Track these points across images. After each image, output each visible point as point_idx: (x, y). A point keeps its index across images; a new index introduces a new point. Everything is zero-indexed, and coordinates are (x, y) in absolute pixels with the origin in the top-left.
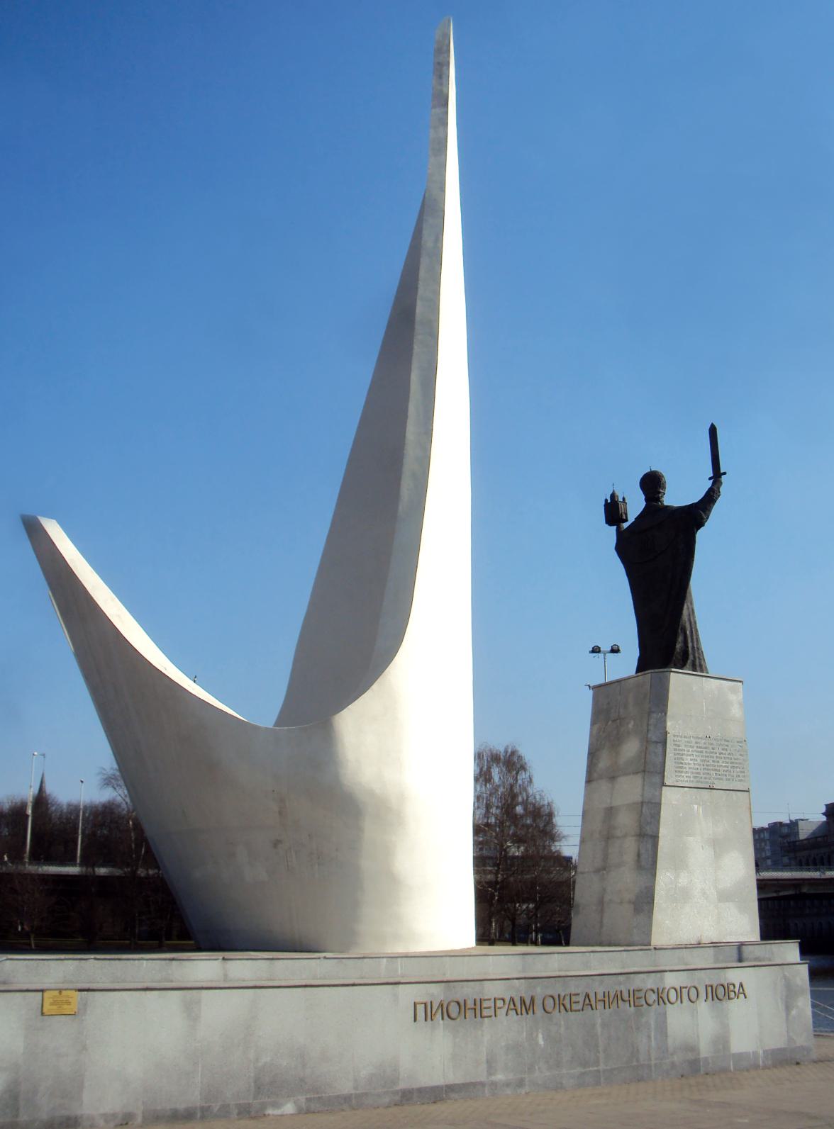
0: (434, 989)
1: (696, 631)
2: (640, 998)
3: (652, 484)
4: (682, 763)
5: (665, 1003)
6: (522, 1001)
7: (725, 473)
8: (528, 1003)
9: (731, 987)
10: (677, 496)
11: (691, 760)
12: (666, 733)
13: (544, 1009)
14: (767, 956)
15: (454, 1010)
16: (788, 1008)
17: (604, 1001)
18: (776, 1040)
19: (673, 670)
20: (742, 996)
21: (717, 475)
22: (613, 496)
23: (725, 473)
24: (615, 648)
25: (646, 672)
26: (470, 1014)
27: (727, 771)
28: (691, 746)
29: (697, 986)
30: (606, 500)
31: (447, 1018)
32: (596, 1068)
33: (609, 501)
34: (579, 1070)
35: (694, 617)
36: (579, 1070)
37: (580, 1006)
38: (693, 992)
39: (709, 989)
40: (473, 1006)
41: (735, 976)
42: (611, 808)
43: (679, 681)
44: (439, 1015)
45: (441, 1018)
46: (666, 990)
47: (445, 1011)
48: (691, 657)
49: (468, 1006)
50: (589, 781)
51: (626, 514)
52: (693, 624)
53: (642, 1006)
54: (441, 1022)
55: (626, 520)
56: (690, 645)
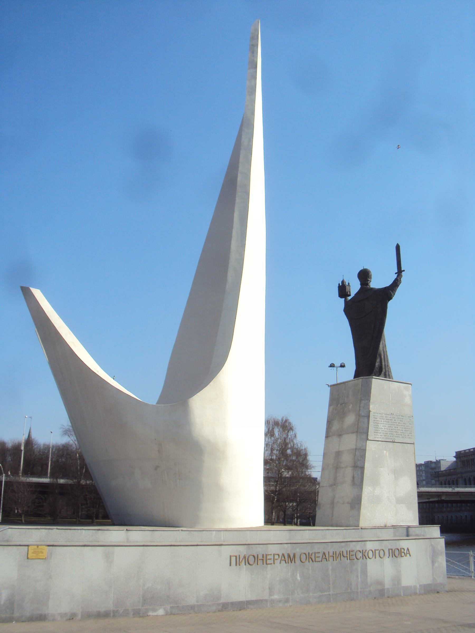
0: (241, 548)
4: (378, 428)
5: (366, 558)
7: (404, 271)
9: (403, 550)
12: (369, 411)
15: (251, 560)
17: (333, 557)
19: (374, 377)
21: (400, 271)
22: (343, 282)
23: (404, 271)
25: (359, 378)
27: (402, 432)
29: (384, 549)
30: (339, 284)
33: (341, 285)
34: (319, 594)
35: (386, 348)
36: (319, 594)
37: (320, 559)
38: (382, 553)
39: (391, 551)
48: (384, 370)
50: (327, 437)
51: (350, 292)
52: (385, 352)
53: (354, 559)
55: (350, 295)
56: (383, 364)
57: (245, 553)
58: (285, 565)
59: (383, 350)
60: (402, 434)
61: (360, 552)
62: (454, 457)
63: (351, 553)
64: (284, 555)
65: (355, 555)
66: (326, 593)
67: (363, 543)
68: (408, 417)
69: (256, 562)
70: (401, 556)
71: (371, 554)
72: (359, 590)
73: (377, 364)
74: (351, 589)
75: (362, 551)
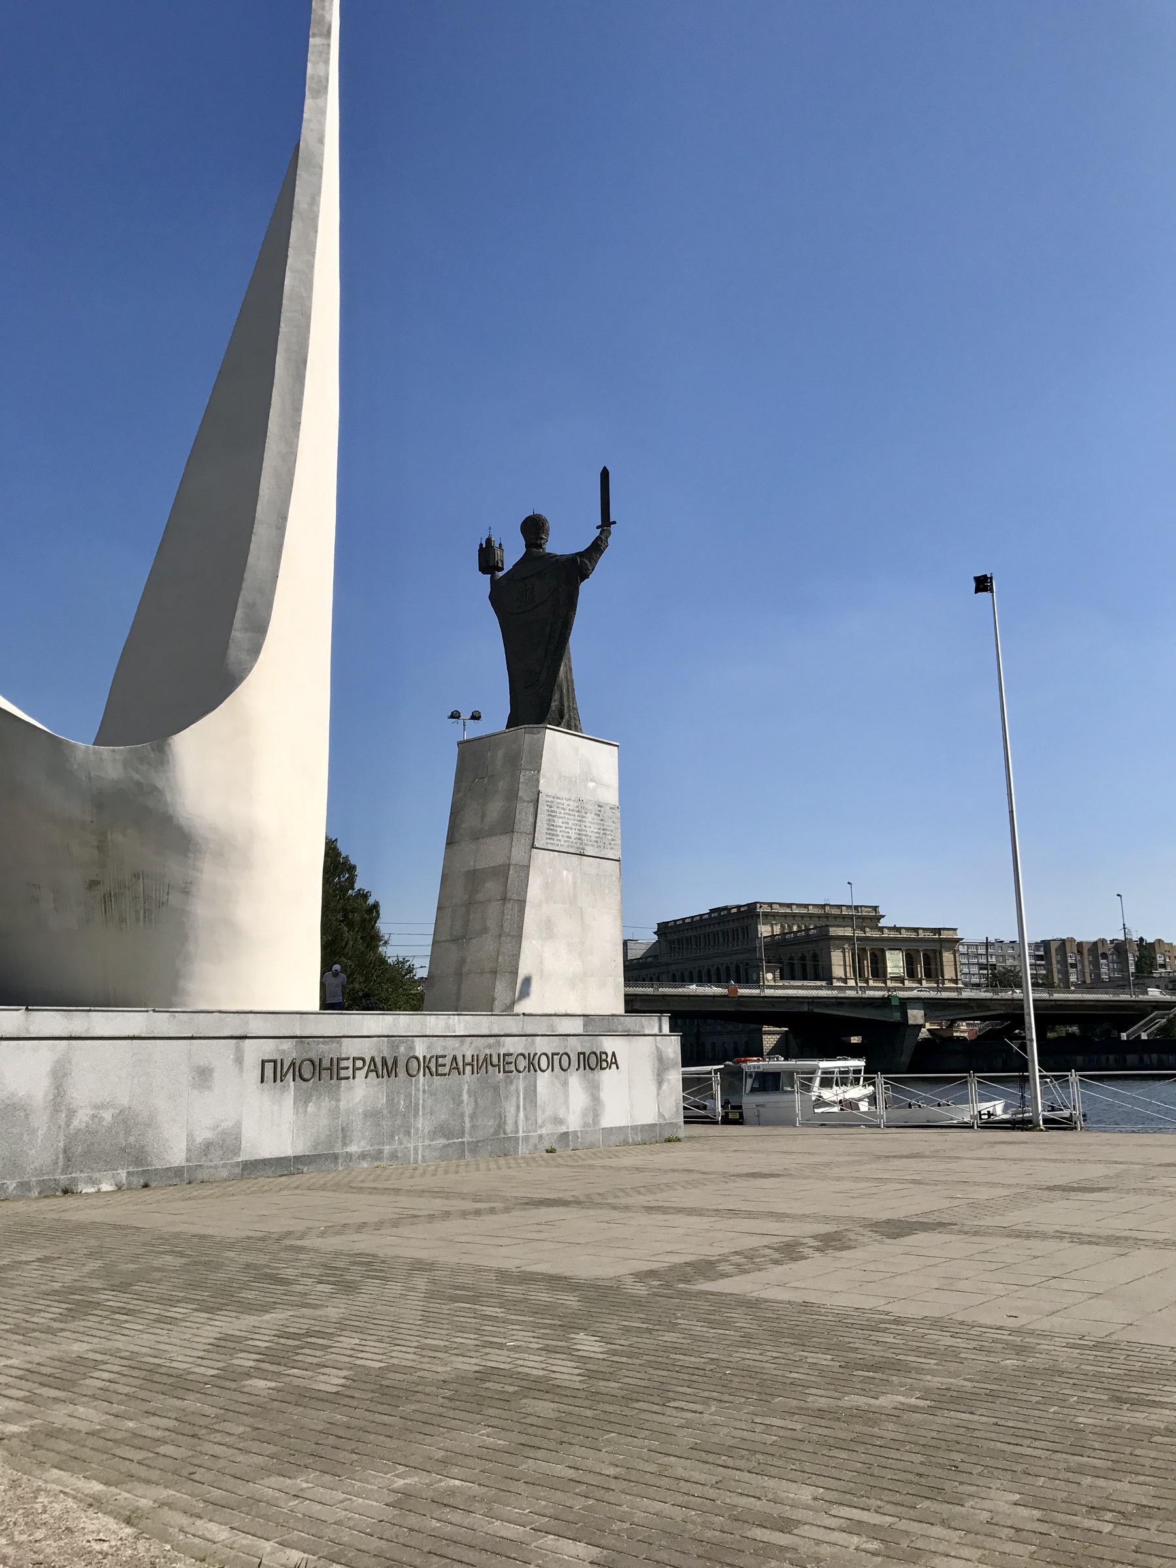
0: (287, 1045)
1: (573, 690)
2: (511, 1063)
3: (534, 528)
4: (553, 826)
5: (536, 1071)
6: (384, 1061)
7: (614, 523)
8: (390, 1065)
9: (604, 1057)
10: (561, 543)
11: (563, 823)
12: (539, 792)
13: (407, 1071)
14: (637, 1029)
15: (307, 1071)
16: (660, 1083)
17: (472, 1065)
18: (647, 1115)
19: (549, 726)
20: (614, 1066)
21: (606, 522)
22: (489, 541)
23: (614, 523)
24: (476, 715)
25: (519, 727)
26: (326, 1074)
27: (598, 837)
28: (563, 808)
29: (570, 1053)
30: (481, 545)
31: (299, 1079)
32: (460, 1140)
33: (484, 546)
34: (443, 1141)
35: (571, 675)
36: (443, 1141)
37: (446, 1070)
38: (565, 1058)
39: (582, 1056)
40: (329, 1066)
41: (609, 1045)
42: (475, 871)
43: (555, 741)
44: (290, 1076)
45: (292, 1079)
46: (538, 1056)
47: (296, 1070)
48: (567, 717)
49: (324, 1066)
50: (450, 842)
51: (502, 562)
52: (570, 682)
53: (512, 1072)
54: (292, 1083)
55: (502, 569)
56: (566, 704)
57: (294, 1055)
58: (376, 1081)
59: (566, 677)
60: (599, 840)
61: (525, 1058)
62: (655, 933)
63: (508, 1059)
64: (374, 1063)
65: (513, 1064)
66: (455, 1141)
67: (530, 1039)
68: (611, 808)
69: (317, 1074)
70: (602, 1068)
71: (544, 1062)
72: (521, 1134)
73: (554, 704)
74: (505, 1133)
75: (527, 1056)
